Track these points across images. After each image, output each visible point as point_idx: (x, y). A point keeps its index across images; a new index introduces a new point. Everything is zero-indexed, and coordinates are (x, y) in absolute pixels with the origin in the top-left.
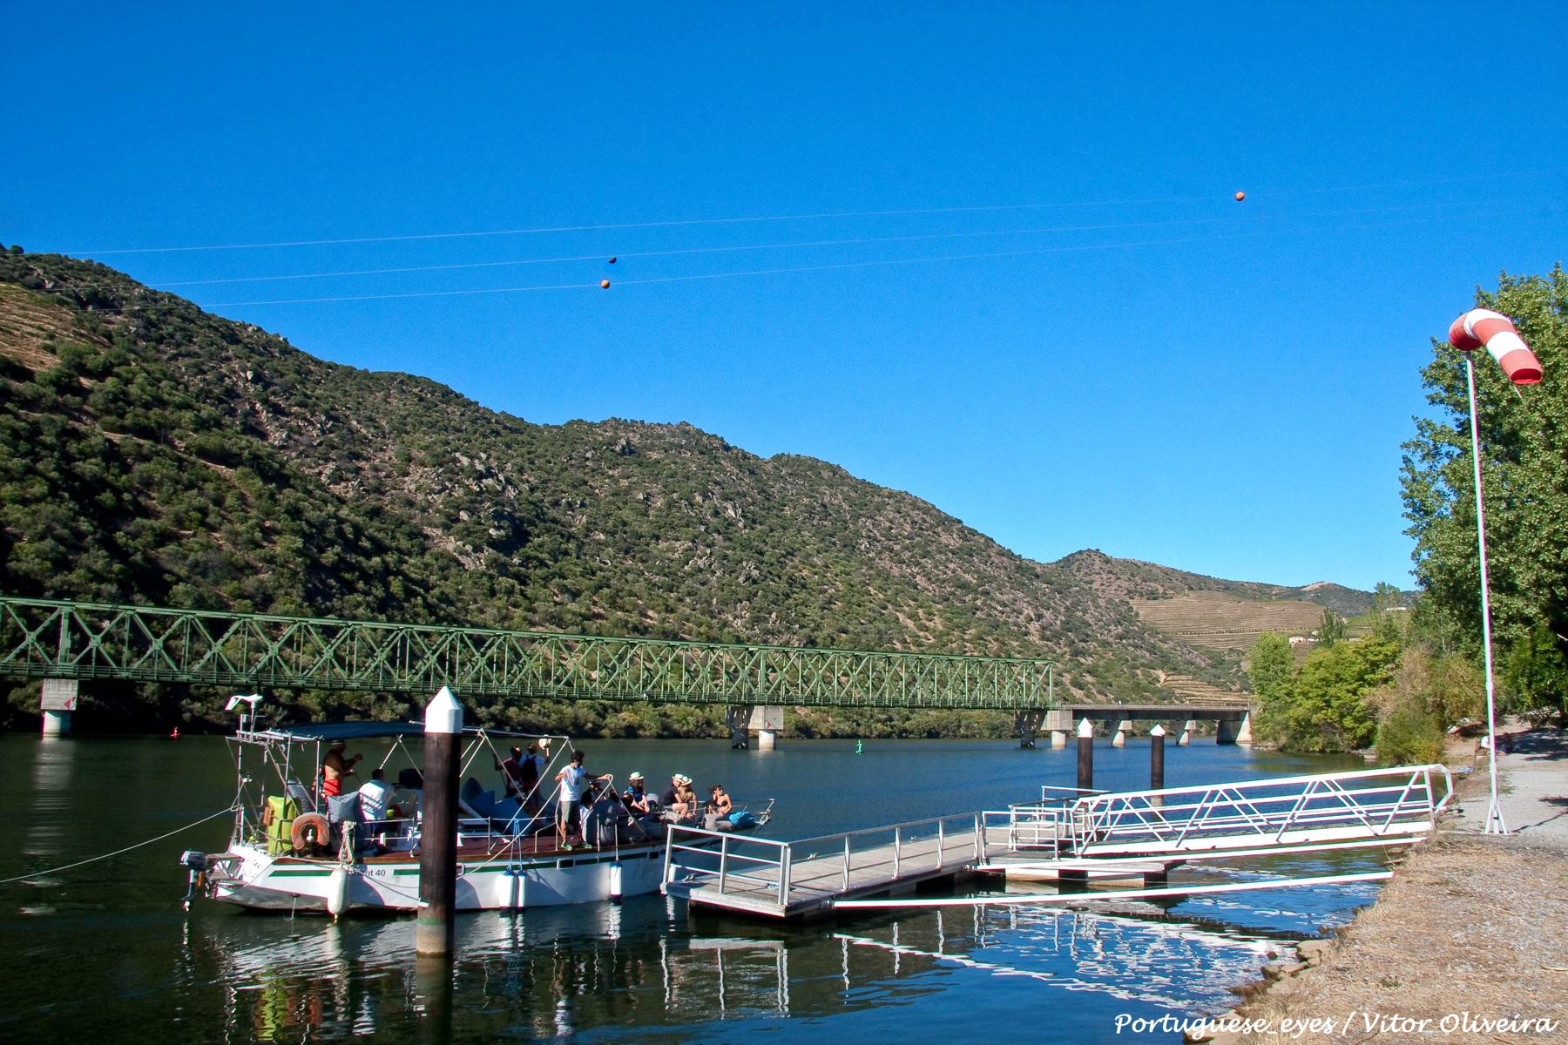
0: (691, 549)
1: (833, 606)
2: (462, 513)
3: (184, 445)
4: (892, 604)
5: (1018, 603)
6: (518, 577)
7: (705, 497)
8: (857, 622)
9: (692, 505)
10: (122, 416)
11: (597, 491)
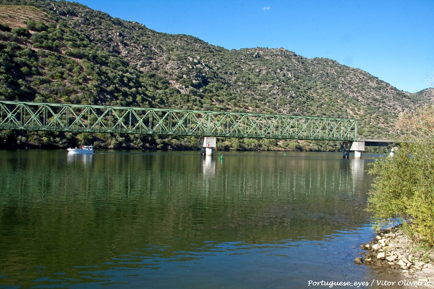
0: (272, 87)
1: (322, 106)
2: (184, 75)
3: (65, 52)
4: (346, 105)
5: (395, 106)
6: (200, 96)
7: (281, 70)
8: (331, 111)
9: (276, 73)
10: (42, 43)
11: (243, 69)
